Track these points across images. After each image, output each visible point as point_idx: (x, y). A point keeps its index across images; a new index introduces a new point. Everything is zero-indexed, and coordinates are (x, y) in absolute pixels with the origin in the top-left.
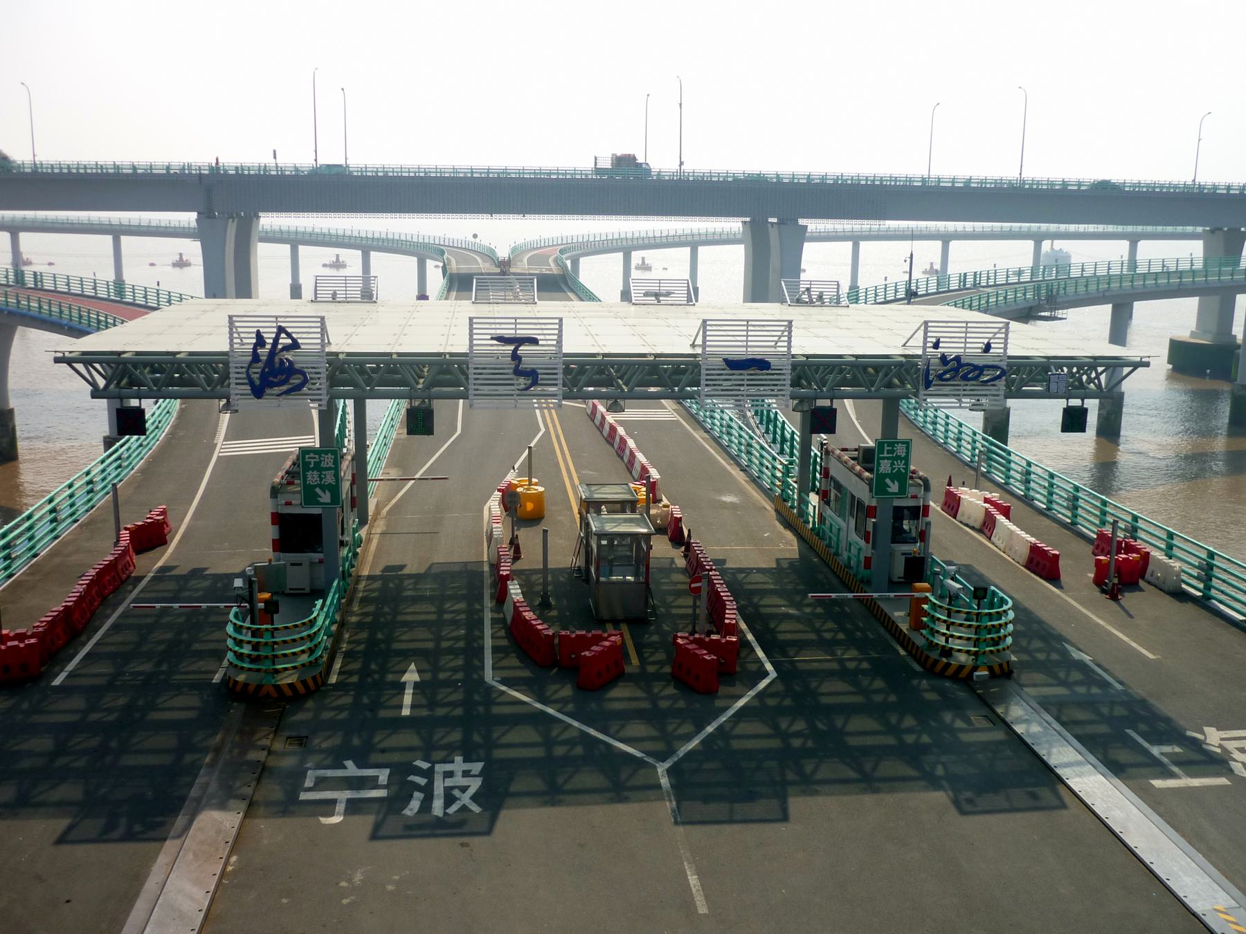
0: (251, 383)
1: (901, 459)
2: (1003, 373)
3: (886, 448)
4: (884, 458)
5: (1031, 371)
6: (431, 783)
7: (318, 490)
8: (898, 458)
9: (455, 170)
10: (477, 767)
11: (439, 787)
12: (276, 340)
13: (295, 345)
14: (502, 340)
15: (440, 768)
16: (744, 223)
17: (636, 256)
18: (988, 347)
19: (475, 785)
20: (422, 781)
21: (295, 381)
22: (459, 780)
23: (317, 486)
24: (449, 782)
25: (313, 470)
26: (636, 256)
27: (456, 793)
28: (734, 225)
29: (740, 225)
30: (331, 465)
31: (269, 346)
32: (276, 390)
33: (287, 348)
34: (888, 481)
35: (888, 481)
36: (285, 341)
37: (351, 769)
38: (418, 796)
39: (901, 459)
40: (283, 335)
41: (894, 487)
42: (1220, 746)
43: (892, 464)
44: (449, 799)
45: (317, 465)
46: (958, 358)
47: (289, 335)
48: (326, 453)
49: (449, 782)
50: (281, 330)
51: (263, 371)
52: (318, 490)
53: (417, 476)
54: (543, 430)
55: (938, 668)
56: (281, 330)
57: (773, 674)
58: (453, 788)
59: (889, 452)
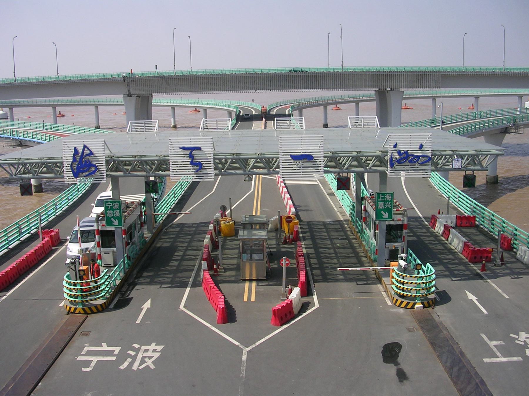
0: (73, 171)
1: (389, 201)
2: (430, 159)
3: (381, 196)
4: (380, 201)
5: (445, 158)
6: (136, 356)
7: (112, 219)
8: (387, 201)
9: (488, 69)
10: (160, 348)
11: (140, 356)
12: (83, 150)
13: (91, 153)
14: (184, 148)
15: (144, 348)
16: (376, 91)
17: (58, 109)
18: (421, 147)
19: (157, 355)
20: (133, 353)
21: (93, 169)
22: (149, 354)
23: (112, 217)
24: (145, 354)
25: (110, 210)
26: (58, 109)
27: (146, 359)
28: (371, 92)
29: (374, 92)
30: (117, 207)
31: (80, 154)
32: (84, 174)
33: (88, 155)
34: (382, 212)
35: (382, 212)
36: (87, 152)
37: (105, 347)
38: (129, 360)
39: (389, 201)
40: (86, 149)
41: (386, 215)
42: (525, 341)
43: (384, 204)
44: (143, 361)
45: (112, 207)
46: (406, 152)
47: (88, 149)
48: (115, 202)
49: (145, 354)
50: (85, 147)
51: (78, 165)
52: (112, 219)
53: (187, 212)
54: (252, 189)
55: (72, 310)
56: (85, 147)
57: (317, 305)
58: (145, 357)
59: (382, 198)
